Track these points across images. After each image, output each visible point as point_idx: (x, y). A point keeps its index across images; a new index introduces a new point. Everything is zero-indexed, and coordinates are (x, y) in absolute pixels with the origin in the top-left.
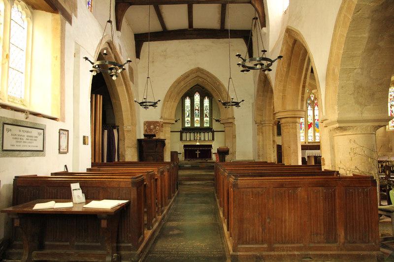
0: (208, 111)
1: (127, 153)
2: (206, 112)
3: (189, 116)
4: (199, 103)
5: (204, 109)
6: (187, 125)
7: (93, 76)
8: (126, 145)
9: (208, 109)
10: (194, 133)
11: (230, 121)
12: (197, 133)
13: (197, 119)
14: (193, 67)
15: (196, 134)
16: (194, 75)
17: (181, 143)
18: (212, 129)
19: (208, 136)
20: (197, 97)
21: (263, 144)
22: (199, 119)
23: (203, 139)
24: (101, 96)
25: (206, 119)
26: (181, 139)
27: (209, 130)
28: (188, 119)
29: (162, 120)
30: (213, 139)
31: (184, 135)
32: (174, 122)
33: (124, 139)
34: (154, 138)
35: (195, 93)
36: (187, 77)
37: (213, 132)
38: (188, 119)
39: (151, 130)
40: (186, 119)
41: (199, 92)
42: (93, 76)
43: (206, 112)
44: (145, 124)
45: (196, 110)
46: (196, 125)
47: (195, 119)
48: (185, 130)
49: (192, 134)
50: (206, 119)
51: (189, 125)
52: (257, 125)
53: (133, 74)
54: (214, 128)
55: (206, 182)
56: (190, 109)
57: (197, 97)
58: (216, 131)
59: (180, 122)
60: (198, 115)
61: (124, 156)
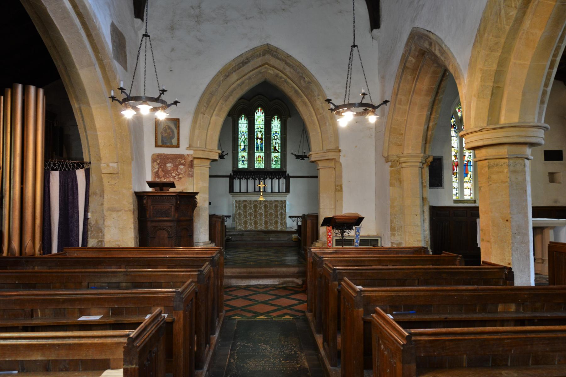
0: (279, 141)
1: (108, 222)
2: (276, 142)
3: (244, 149)
4: (263, 126)
5: (272, 136)
6: (243, 165)
8: (106, 206)
9: (279, 136)
11: (331, 155)
12: (260, 179)
13: (259, 154)
14: (256, 43)
15: (257, 181)
16: (258, 61)
17: (230, 196)
18: (286, 172)
19: (278, 184)
20: (260, 117)
21: (264, 187)
22: (262, 154)
23: (269, 190)
24: (41, 92)
25: (276, 155)
26: (231, 190)
27: (280, 174)
28: (243, 155)
29: (191, 152)
30: (288, 190)
31: (236, 182)
32: (217, 158)
33: (103, 191)
34: (171, 190)
35: (257, 108)
36: (244, 63)
37: (288, 178)
38: (243, 155)
39: (167, 172)
40: (240, 154)
41: (263, 108)
43: (276, 142)
44: (154, 160)
45: (257, 138)
46: (257, 166)
47: (257, 154)
48: (238, 174)
49: (251, 182)
50: (276, 155)
51: (246, 166)
52: (390, 163)
53: (124, 47)
54: (290, 171)
55: (282, 280)
56: (246, 137)
57: (260, 117)
59: (229, 159)
60: (262, 149)
61: (100, 230)
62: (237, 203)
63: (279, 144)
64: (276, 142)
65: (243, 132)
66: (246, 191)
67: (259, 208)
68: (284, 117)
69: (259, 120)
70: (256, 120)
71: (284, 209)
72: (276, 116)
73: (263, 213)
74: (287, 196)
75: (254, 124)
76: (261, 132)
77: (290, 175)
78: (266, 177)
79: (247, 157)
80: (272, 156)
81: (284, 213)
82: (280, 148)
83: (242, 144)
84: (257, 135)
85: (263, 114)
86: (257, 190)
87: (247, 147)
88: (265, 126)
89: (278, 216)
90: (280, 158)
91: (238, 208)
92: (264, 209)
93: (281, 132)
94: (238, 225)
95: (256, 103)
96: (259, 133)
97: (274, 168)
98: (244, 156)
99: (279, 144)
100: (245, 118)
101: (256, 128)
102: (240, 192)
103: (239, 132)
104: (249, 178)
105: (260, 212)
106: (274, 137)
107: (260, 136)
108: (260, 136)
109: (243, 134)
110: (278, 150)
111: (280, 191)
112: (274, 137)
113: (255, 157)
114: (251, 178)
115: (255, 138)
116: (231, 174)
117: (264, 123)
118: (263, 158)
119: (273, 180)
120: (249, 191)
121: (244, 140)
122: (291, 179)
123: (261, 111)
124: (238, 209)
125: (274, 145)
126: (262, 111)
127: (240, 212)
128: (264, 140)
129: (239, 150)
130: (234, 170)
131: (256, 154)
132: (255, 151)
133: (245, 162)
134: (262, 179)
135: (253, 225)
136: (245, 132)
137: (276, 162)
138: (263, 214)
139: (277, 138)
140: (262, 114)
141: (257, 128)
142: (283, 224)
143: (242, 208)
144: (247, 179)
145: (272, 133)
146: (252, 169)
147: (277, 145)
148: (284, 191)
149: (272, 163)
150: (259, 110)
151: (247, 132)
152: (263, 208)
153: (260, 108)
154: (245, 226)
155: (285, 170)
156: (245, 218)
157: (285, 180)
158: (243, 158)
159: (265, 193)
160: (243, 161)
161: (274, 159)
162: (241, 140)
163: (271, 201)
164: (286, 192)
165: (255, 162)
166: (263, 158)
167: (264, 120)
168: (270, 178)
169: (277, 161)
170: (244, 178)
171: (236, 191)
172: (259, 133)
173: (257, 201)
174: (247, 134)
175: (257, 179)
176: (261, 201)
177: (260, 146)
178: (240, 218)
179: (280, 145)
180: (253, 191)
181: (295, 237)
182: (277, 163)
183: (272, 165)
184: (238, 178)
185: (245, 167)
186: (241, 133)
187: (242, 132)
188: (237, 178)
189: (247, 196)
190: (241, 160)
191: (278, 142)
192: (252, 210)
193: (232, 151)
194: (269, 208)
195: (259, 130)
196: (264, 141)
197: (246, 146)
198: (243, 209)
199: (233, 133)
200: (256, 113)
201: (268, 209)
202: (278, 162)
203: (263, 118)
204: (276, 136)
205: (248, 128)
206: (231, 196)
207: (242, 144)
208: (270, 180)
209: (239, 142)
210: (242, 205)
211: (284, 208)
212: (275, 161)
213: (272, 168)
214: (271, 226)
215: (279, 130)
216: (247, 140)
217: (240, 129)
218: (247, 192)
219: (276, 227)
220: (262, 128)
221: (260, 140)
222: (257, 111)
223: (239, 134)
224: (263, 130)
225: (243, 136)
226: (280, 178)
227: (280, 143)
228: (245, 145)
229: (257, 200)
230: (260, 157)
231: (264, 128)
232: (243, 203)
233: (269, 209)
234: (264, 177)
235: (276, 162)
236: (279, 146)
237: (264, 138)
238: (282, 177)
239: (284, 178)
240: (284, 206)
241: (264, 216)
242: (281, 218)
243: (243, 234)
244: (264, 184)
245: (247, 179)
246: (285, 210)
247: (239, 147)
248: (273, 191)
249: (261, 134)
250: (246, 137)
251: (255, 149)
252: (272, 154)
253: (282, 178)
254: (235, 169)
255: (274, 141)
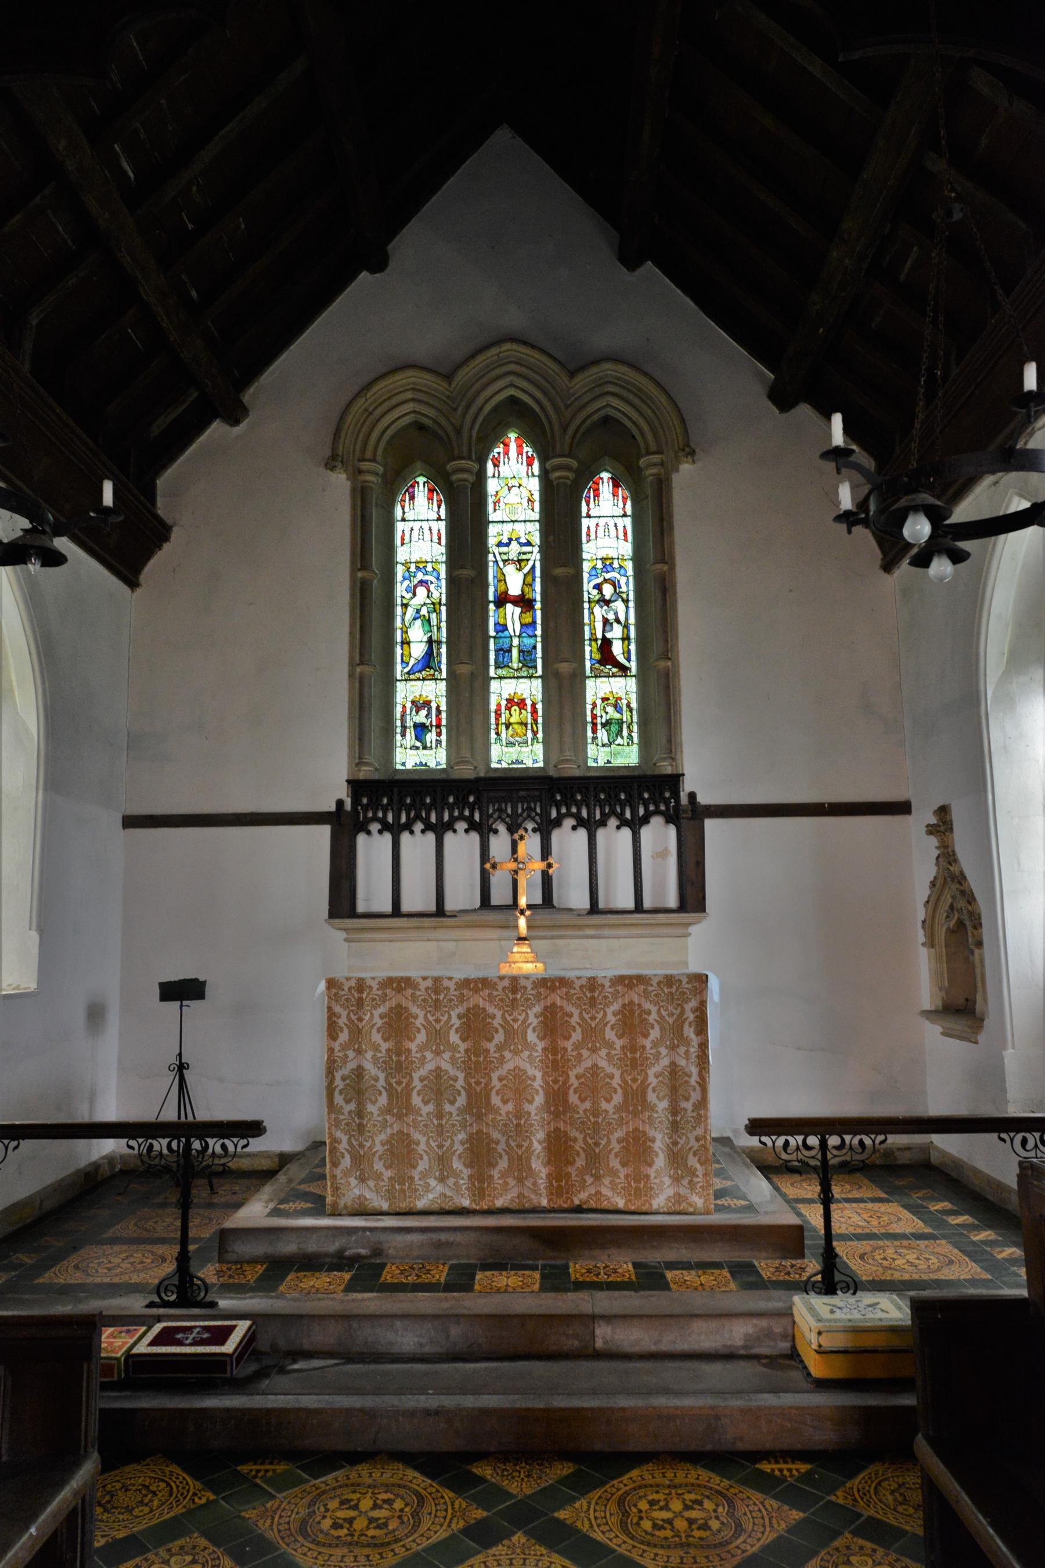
0: (625, 611)
3: (429, 660)
5: (588, 587)
7: (42, 566)
9: (628, 586)
10: (483, 830)
15: (500, 844)
17: (335, 935)
18: (674, 781)
22: (531, 689)
40: (405, 692)
42: (42, 566)
45: (502, 600)
47: (500, 690)
56: (440, 592)
58: (493, 522)
60: (527, 656)
62: (336, 998)
63: (626, 626)
64: (611, 617)
65: (421, 565)
66: (432, 907)
67: (499, 1037)
68: (656, 458)
69: (513, 497)
70: (491, 500)
71: (695, 1040)
72: (605, 475)
73: (537, 1076)
74: (692, 929)
75: (480, 522)
76: (520, 562)
77: (702, 799)
78: (554, 814)
79: (443, 708)
80: (589, 699)
81: (694, 1070)
82: (633, 647)
83: (417, 634)
84: (502, 579)
85: (530, 464)
86: (499, 895)
87: (444, 649)
88: (545, 532)
89: (651, 1097)
90: (634, 705)
91: (344, 1036)
92: (540, 1045)
93: (637, 558)
94: (346, 1174)
95: (490, 390)
96: (510, 570)
97: (601, 763)
98: (427, 703)
99: (626, 626)
100: (431, 491)
101: (492, 541)
102: (397, 911)
103: (400, 570)
104: (450, 826)
105: (510, 1065)
106: (598, 587)
107: (515, 590)
108: (515, 590)
109: (420, 576)
110: (621, 659)
111: (647, 904)
112: (598, 587)
113: (493, 707)
114: (461, 826)
115: (491, 598)
116: (340, 803)
117: (536, 516)
118: (534, 711)
119: (556, 836)
120: (449, 906)
121: (424, 611)
122: (711, 825)
123: (519, 447)
124: (344, 1047)
125: (599, 635)
126: (528, 450)
127: (359, 1071)
128: (538, 606)
129: (399, 667)
130: (361, 776)
131: (494, 685)
132: (492, 672)
133: (431, 737)
134: (530, 826)
135: (456, 1175)
136: (429, 568)
137: (614, 728)
138: (538, 1083)
139: (617, 593)
140: (524, 468)
141: (500, 544)
142: (693, 1161)
143: (377, 1037)
144: (440, 830)
145: (586, 566)
146: (466, 772)
147: (616, 632)
148: (672, 902)
149: (590, 734)
150: (506, 445)
151: (443, 569)
152: (531, 1037)
153: (513, 436)
154: (403, 1178)
155: (669, 770)
156: (399, 1117)
157: (672, 831)
158: (424, 713)
159: (545, 917)
160: (421, 729)
161: (598, 711)
162: (410, 612)
163: (592, 984)
164: (683, 907)
165: (493, 736)
166: (534, 711)
167: (537, 497)
168: (581, 823)
169: (620, 723)
170: (419, 826)
171: (376, 908)
172: (510, 570)
173: (485, 983)
174: (443, 575)
175: (502, 828)
176: (514, 979)
177: (516, 642)
178: (360, 1113)
179: (632, 634)
180: (477, 904)
181: (827, 1342)
182: (620, 733)
183: (591, 750)
184: (386, 827)
185: (432, 765)
186: (409, 576)
187: (413, 569)
188: (375, 827)
189: (440, 934)
190: (409, 723)
191: (622, 619)
192: (454, 1049)
193: (352, 665)
194: (577, 1036)
195: (513, 555)
196: (539, 614)
197: (439, 643)
198: (384, 1046)
199: (353, 562)
200: (490, 465)
201: (569, 1045)
202: (625, 733)
203: (534, 485)
204: (614, 584)
205: (450, 547)
206: (343, 935)
207: (417, 634)
208: (388, 837)
209: (398, 623)
210: (375, 1016)
211: (689, 1032)
212: (606, 724)
213: (591, 763)
214: (594, 1050)
215: (626, 549)
216: (444, 609)
217: (402, 554)
218: (440, 911)
219: (640, 1184)
220: (529, 544)
221: (518, 610)
222: (500, 449)
223: (399, 578)
224: (536, 549)
225: (421, 591)
226: (645, 820)
227: (632, 620)
228: (430, 641)
229: (491, 974)
230: (516, 702)
231: (536, 539)
232: (384, 998)
233: (577, 1047)
234: (546, 813)
235: (614, 728)
236: (626, 639)
237: (538, 598)
238: (657, 812)
239: (669, 820)
240: (691, 1017)
241: (539, 1099)
242: (674, 1110)
243: (377, 1252)
244: (546, 852)
245: (440, 830)
246: (703, 1046)
247: (398, 651)
248: (602, 905)
249: (520, 576)
250: (436, 595)
251: (492, 662)
252: (590, 683)
253: (657, 821)
254: (365, 773)
255: (599, 611)
